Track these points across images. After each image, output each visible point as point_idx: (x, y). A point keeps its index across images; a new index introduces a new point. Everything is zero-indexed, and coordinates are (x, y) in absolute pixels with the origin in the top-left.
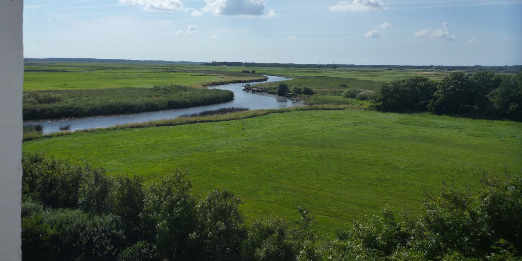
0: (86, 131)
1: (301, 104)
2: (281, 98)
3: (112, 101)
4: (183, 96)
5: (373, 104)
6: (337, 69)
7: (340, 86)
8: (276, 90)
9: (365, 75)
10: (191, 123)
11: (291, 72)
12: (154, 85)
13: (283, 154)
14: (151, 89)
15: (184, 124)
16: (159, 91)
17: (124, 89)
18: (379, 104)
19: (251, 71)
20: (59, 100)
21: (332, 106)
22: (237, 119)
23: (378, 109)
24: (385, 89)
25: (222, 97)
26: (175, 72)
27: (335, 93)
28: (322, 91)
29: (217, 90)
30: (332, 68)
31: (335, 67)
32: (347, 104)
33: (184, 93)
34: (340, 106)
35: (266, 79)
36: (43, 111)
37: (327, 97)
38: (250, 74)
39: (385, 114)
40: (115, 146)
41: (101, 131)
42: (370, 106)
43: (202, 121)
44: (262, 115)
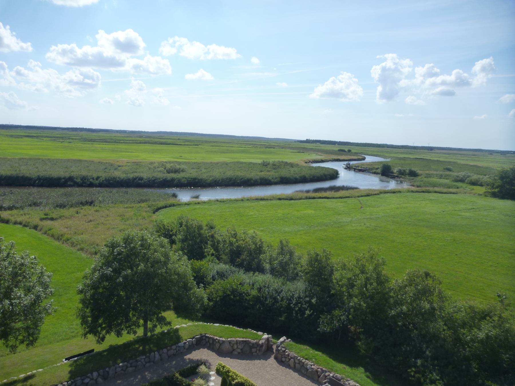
0: (217, 201)
1: (405, 186)
2: (384, 178)
3: (230, 174)
4: (292, 172)
5: (490, 191)
6: (433, 151)
7: (444, 169)
8: (379, 171)
9: (465, 158)
10: (310, 198)
11: (387, 152)
12: (262, 160)
13: (414, 235)
14: (260, 164)
15: (304, 199)
16: (269, 166)
17: (235, 163)
18: (496, 190)
19: (346, 150)
20: (183, 171)
21: (445, 190)
22: (352, 197)
23: (494, 195)
24: (503, 176)
25: (328, 175)
26: (274, 148)
27: (441, 177)
28: (427, 174)
29: (319, 167)
30: (428, 150)
31: (431, 149)
32: (458, 188)
33: (292, 169)
34: (451, 190)
35: (364, 159)
36: (173, 180)
37: (435, 180)
38: (348, 152)
39: (502, 200)
40: (248, 216)
41: (230, 201)
42: (485, 192)
43: (320, 198)
44: (376, 194)
